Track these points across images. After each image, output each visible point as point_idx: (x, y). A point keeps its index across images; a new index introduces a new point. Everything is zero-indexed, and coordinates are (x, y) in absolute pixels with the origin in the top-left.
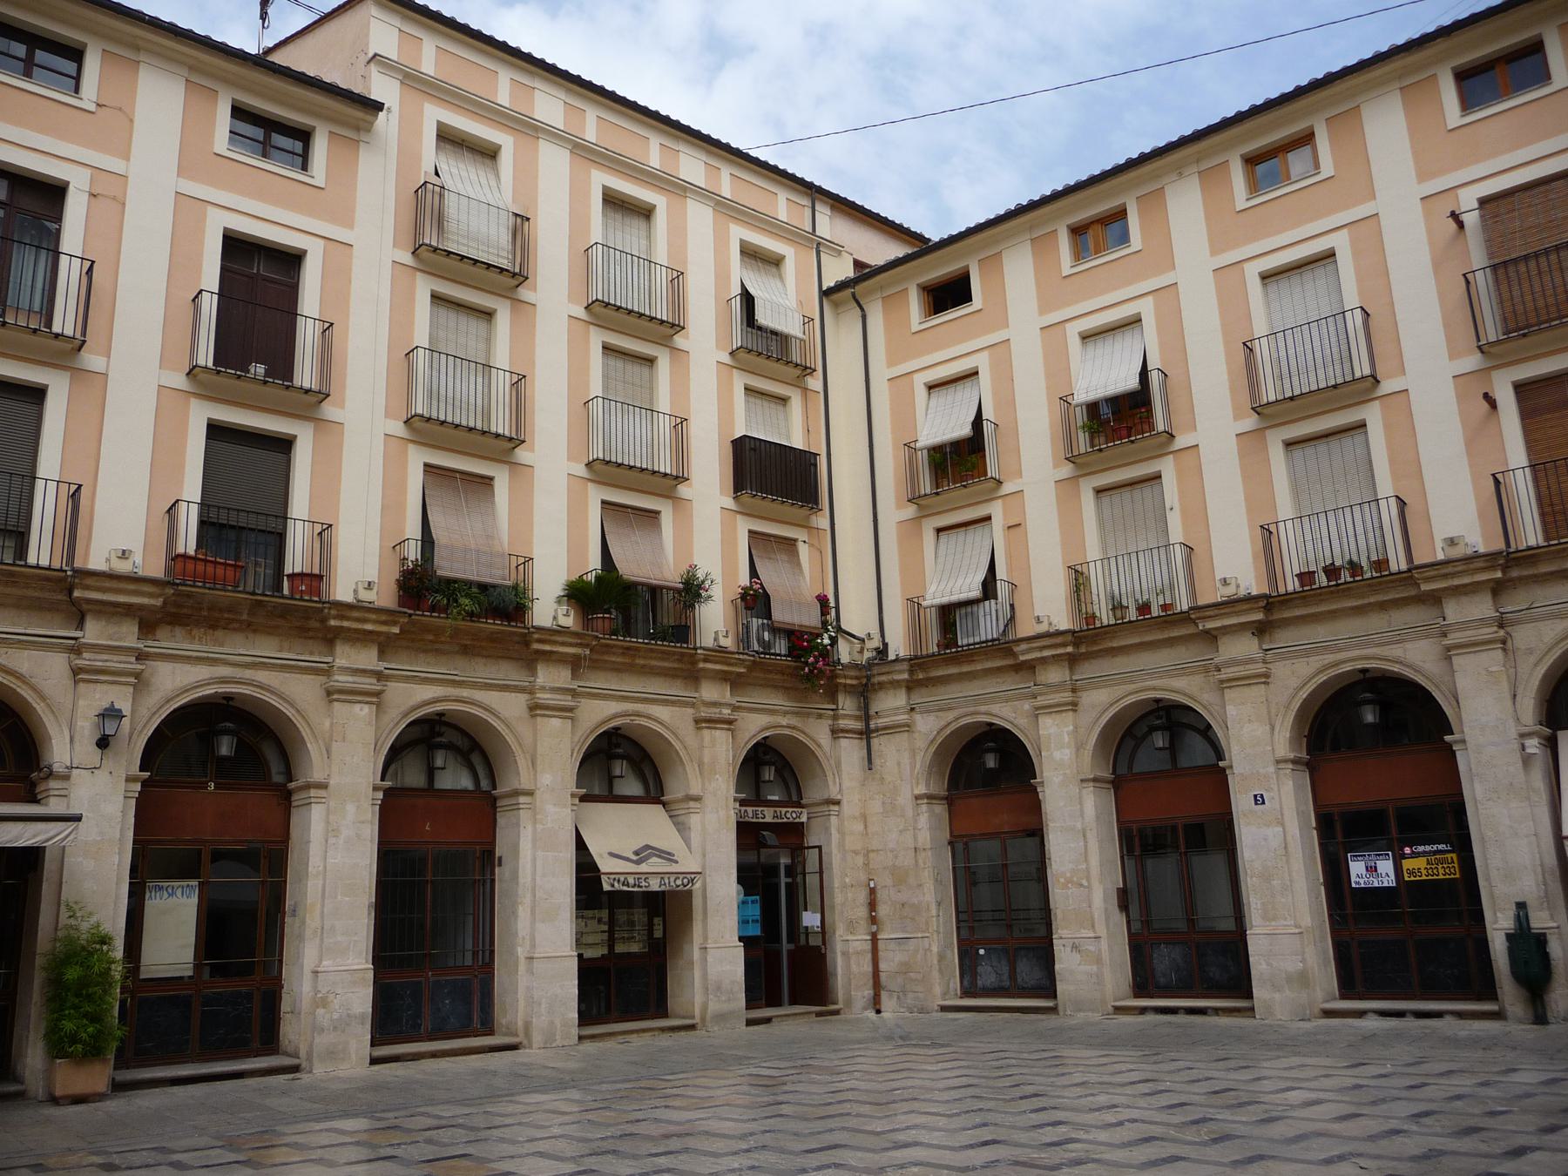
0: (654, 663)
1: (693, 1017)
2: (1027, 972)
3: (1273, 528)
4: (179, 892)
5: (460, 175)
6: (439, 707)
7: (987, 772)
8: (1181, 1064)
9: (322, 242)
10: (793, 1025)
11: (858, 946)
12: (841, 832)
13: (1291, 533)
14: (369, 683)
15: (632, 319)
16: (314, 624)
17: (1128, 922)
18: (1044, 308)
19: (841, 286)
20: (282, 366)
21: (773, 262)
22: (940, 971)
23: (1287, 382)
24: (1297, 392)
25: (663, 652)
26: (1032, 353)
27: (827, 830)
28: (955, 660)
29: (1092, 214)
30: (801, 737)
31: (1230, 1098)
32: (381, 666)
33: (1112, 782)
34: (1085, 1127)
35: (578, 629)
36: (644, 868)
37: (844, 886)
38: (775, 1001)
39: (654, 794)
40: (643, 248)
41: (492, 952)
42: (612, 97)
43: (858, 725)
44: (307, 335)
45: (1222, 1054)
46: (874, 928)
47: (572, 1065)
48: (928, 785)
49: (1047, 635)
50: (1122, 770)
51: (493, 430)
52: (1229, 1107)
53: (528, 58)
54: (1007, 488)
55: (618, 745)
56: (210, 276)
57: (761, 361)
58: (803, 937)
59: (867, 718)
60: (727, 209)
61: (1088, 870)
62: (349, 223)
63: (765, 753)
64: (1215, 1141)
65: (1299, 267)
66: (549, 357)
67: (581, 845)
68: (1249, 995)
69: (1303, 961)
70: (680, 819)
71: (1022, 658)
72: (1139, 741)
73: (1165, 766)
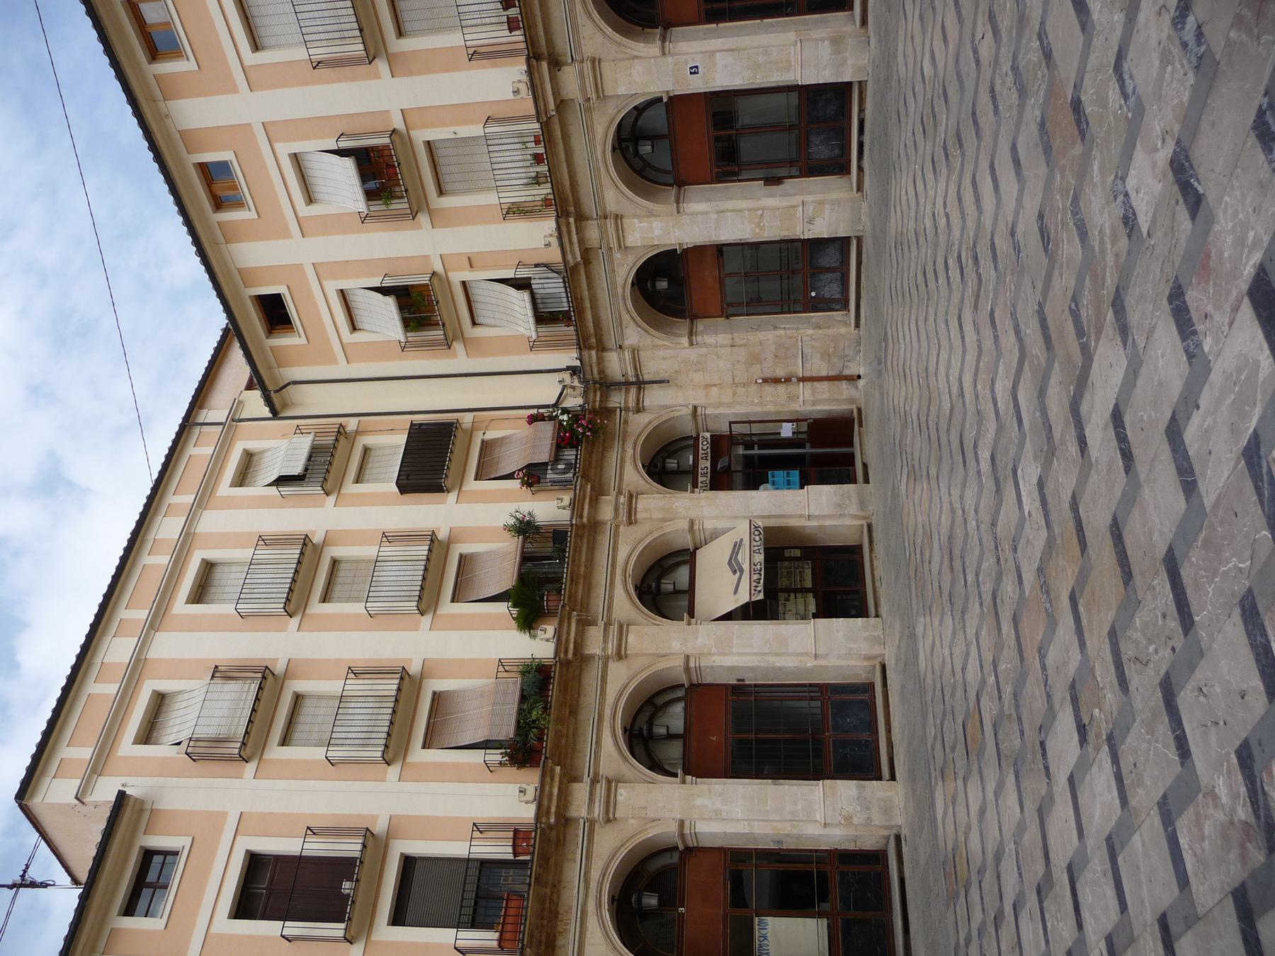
0: (583, 559)
1: (874, 667)
2: (829, 258)
3: (471, 51)
4: (763, 932)
5: (180, 724)
6: (619, 732)
7: (671, 288)
8: (902, 151)
9: (238, 838)
10: (868, 446)
11: (808, 392)
12: (719, 405)
13: (475, 36)
14: (601, 789)
15: (300, 578)
16: (553, 834)
17: (791, 177)
18: (286, 235)
19: (269, 401)
20: (343, 867)
21: (249, 459)
22: (828, 328)
23: (346, 34)
24: (356, 26)
25: (575, 551)
26: (323, 245)
27: (716, 416)
28: (580, 312)
29: (204, 192)
30: (643, 437)
31: (929, 122)
32: (587, 780)
33: (679, 187)
34: (949, 245)
35: (556, 621)
36: (746, 566)
37: (761, 403)
38: (850, 459)
39: (687, 557)
40: (239, 569)
41: (811, 685)
42: (108, 597)
43: (633, 391)
44: (318, 847)
45: (894, 116)
46: (794, 379)
47: (897, 626)
48: (681, 336)
49: (560, 238)
50: (670, 179)
51: (394, 693)
52: (935, 126)
53: (76, 669)
54: (438, 268)
55: (650, 587)
56: (271, 928)
57: (333, 470)
58: (801, 436)
59: (627, 384)
60: (204, 498)
61: (749, 210)
62: (224, 815)
63: (656, 466)
64: (961, 146)
65: (247, 18)
66: (331, 648)
67: (728, 617)
68: (850, 84)
69: (823, 40)
70: (708, 536)
71: (579, 259)
72: (647, 164)
73: (669, 144)
